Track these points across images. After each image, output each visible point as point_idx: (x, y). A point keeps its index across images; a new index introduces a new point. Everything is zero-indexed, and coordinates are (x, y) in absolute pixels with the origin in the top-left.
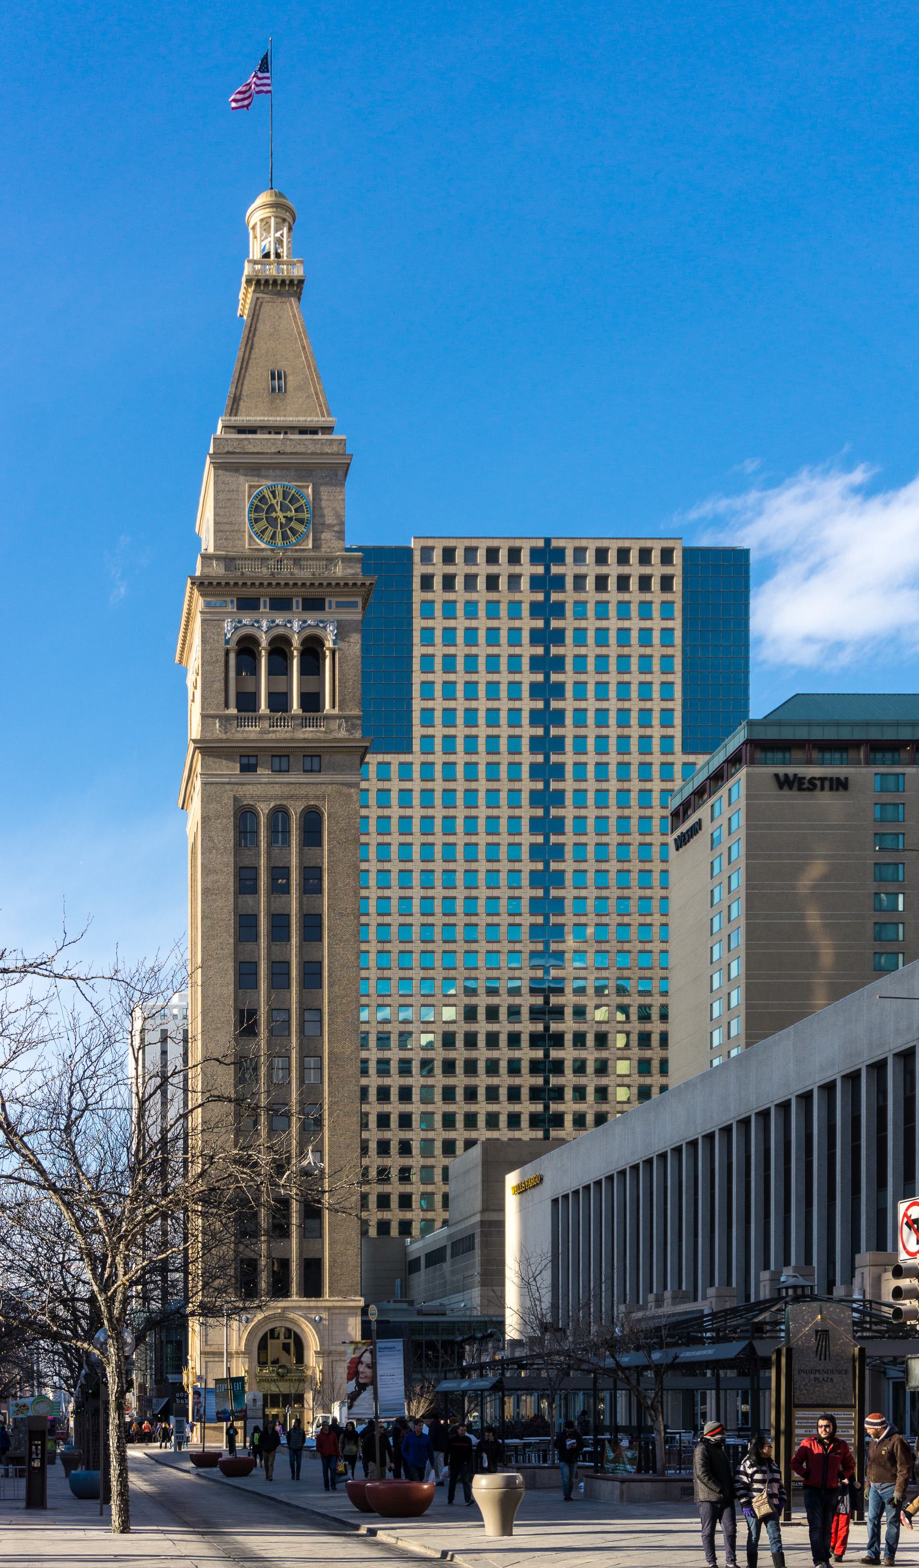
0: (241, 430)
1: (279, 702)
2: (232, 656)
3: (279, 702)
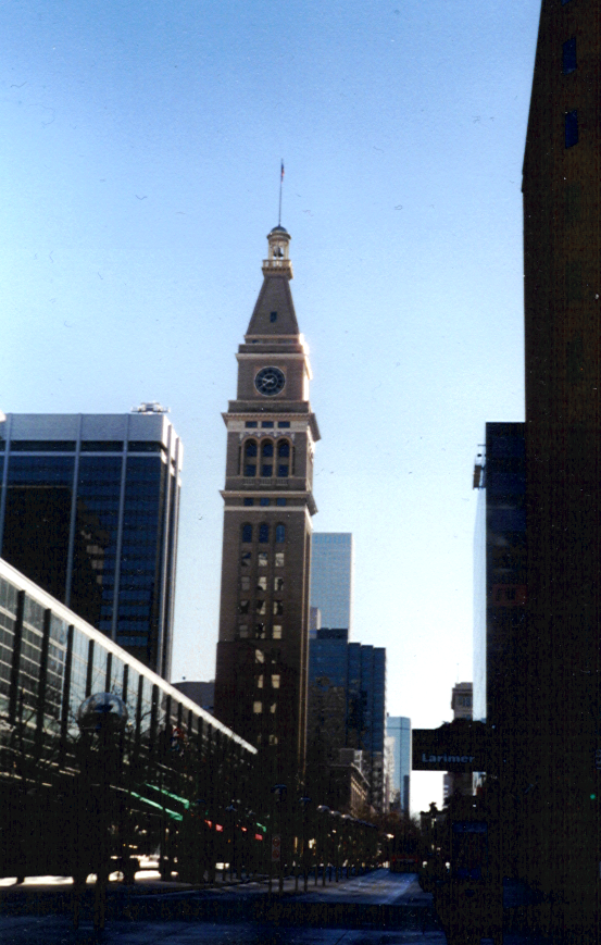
0: (255, 341)
2: (243, 450)
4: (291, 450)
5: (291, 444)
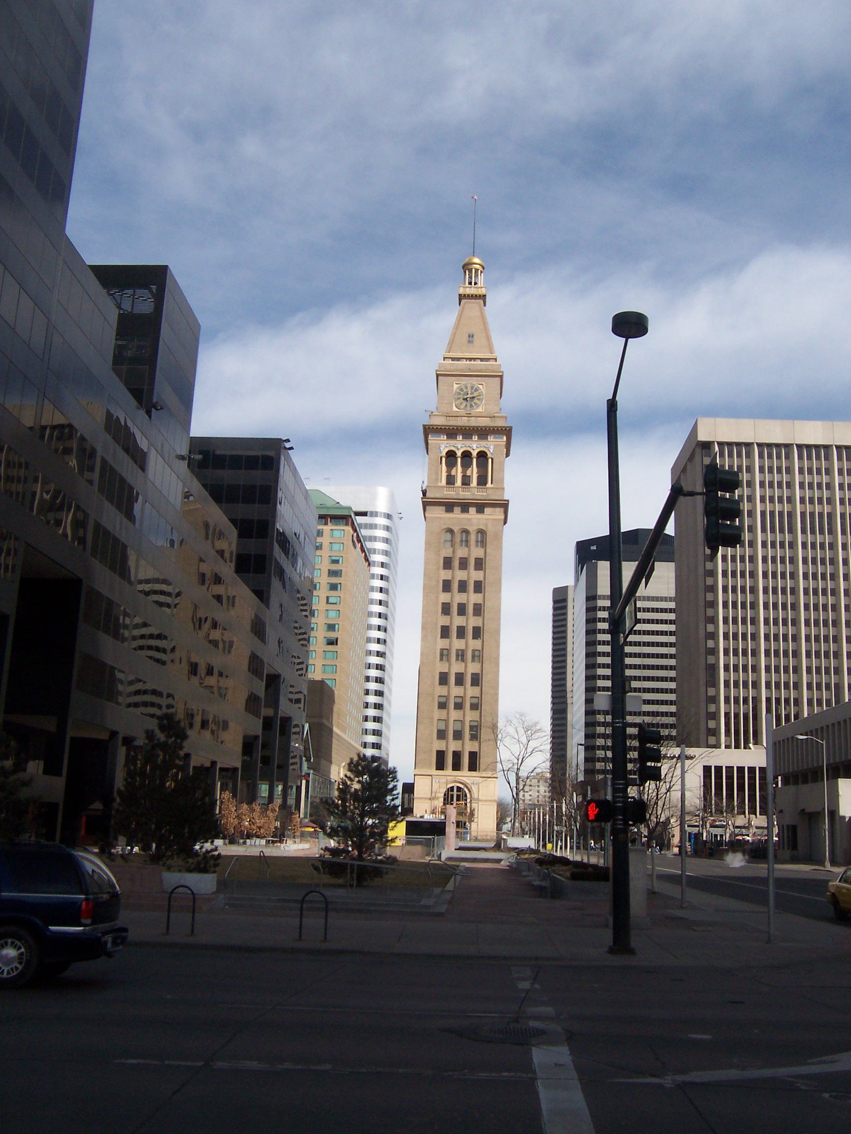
1: (466, 481)
2: (444, 459)
3: (466, 481)
4: (490, 460)
5: (489, 455)
